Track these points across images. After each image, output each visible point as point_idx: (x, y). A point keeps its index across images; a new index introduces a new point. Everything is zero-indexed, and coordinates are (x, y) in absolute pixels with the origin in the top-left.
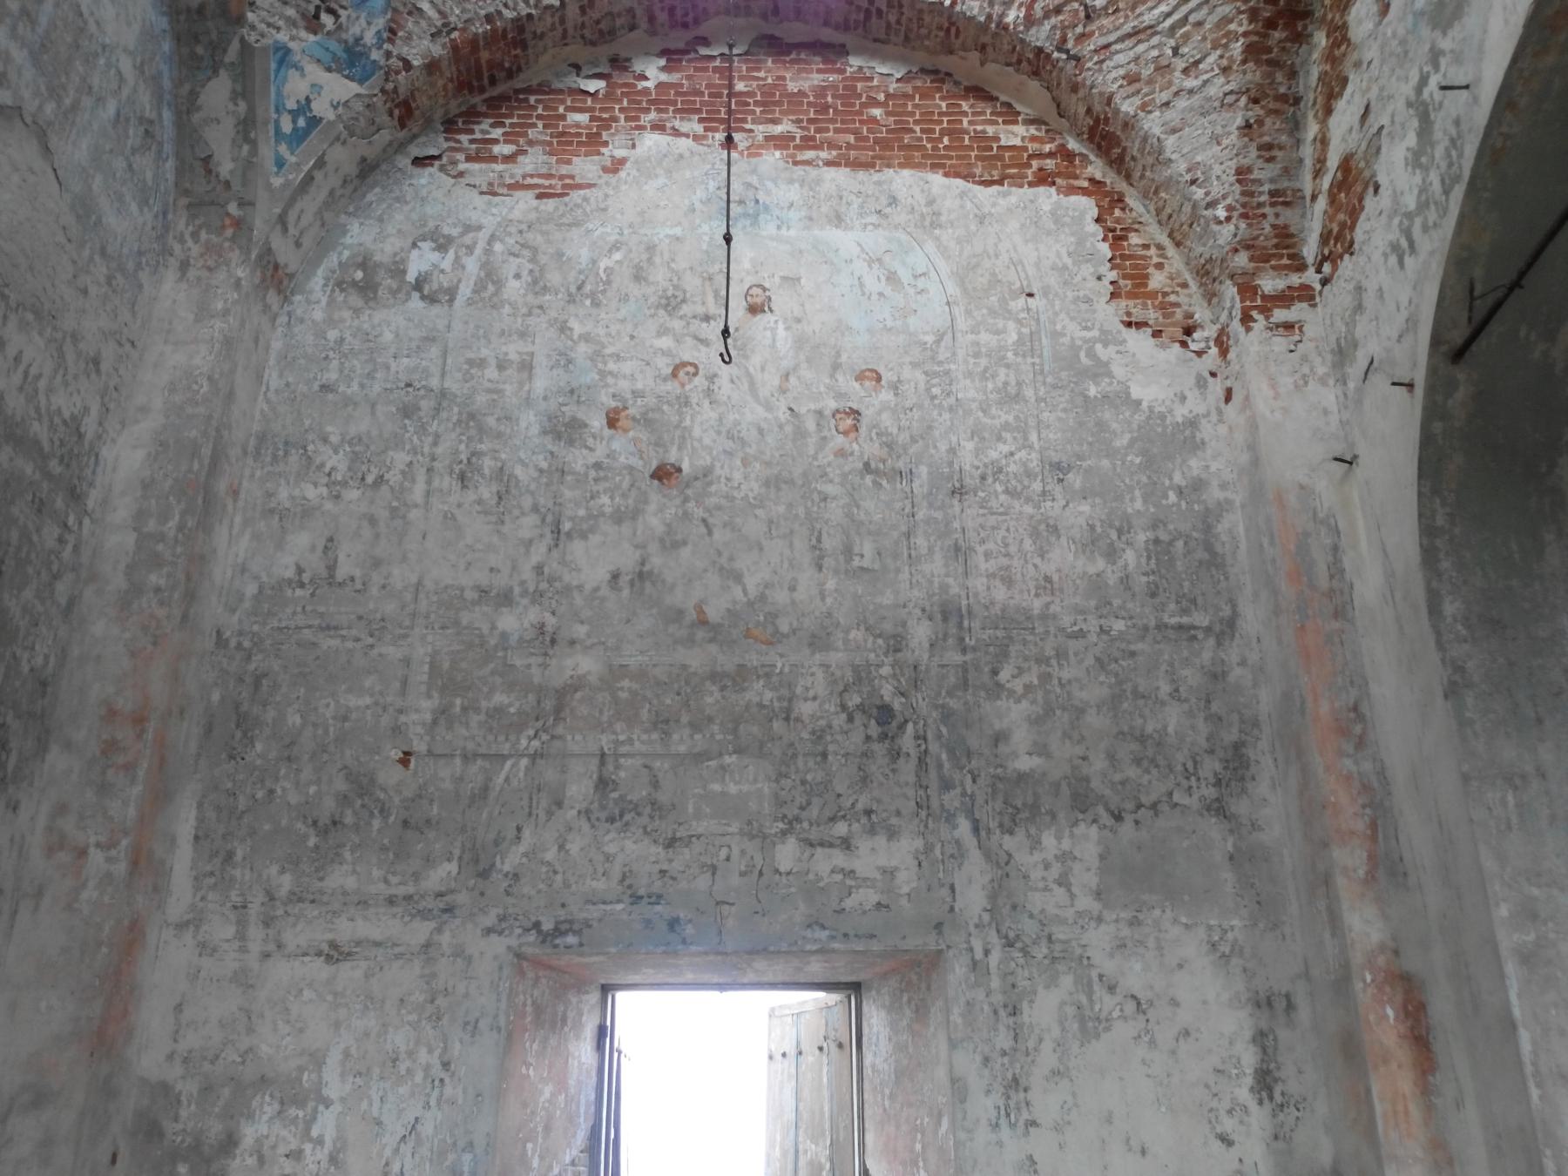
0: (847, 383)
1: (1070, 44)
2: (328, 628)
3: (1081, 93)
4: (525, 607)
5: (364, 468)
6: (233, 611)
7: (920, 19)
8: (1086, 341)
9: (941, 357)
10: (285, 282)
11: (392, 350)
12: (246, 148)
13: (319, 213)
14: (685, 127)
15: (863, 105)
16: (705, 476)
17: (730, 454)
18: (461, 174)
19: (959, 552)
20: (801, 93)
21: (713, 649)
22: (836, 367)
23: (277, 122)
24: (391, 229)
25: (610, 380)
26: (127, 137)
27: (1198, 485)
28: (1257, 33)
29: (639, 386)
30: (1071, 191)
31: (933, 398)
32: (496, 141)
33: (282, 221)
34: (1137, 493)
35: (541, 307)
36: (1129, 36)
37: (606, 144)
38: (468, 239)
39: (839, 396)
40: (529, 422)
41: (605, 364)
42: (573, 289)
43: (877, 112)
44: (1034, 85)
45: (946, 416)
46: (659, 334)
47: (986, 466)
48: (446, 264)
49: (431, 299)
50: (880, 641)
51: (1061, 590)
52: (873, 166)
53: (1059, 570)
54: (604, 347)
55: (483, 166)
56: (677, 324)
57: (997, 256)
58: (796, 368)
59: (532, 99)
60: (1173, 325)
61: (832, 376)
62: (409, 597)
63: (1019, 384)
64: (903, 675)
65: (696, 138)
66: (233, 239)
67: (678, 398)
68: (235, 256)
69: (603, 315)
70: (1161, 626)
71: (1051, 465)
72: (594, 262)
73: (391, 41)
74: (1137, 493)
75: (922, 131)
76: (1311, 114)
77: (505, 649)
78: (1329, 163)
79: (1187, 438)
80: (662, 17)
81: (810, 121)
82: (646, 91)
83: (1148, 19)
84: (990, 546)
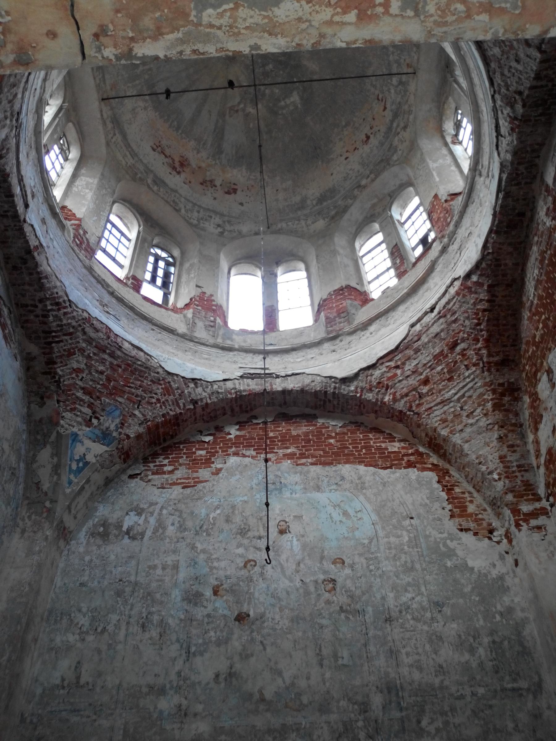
0: (328, 565)
1: (414, 408)
2: (75, 711)
3: (422, 428)
4: (172, 696)
5: (97, 624)
6: (30, 702)
7: (347, 402)
8: (441, 539)
9: (373, 550)
10: (68, 536)
11: (114, 564)
12: (55, 477)
13: (86, 503)
14: (248, 453)
15: (326, 438)
16: (261, 618)
17: (273, 605)
18: (149, 481)
19: (393, 653)
20: (298, 435)
21: (268, 715)
22: (322, 558)
23: (70, 465)
24: (117, 507)
25: (215, 571)
26: (3, 476)
27: (510, 610)
28: (497, 399)
29: (228, 573)
30: (424, 469)
31: (371, 571)
32: (165, 465)
33: (69, 508)
34: (480, 616)
35: (183, 538)
36: (440, 403)
37: (213, 463)
38: (151, 509)
39: (325, 572)
40: (176, 595)
41: (212, 563)
42: (198, 528)
43: (332, 441)
44: (400, 425)
45: (378, 580)
46: (238, 547)
47: (401, 605)
48: (141, 522)
49: (133, 538)
50: (356, 707)
51: (448, 672)
52: (332, 464)
53: (446, 661)
54: (212, 555)
55: (159, 476)
56: (246, 542)
57: (393, 501)
58: (303, 559)
59: (181, 446)
60: (483, 529)
61: (321, 563)
62: (114, 692)
63: (412, 562)
64: (370, 726)
65: (253, 457)
66: (46, 518)
67: (247, 578)
68: (47, 525)
69: (212, 540)
70: (503, 690)
71: (434, 603)
72: (208, 515)
73: (121, 428)
74: (480, 616)
75: (353, 447)
76: (529, 431)
77: (161, 720)
78: (542, 452)
79: (499, 586)
80: (237, 409)
81: (303, 447)
82: (230, 439)
83: (447, 396)
84: (408, 649)
